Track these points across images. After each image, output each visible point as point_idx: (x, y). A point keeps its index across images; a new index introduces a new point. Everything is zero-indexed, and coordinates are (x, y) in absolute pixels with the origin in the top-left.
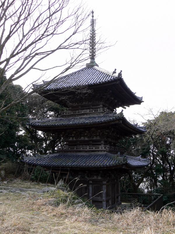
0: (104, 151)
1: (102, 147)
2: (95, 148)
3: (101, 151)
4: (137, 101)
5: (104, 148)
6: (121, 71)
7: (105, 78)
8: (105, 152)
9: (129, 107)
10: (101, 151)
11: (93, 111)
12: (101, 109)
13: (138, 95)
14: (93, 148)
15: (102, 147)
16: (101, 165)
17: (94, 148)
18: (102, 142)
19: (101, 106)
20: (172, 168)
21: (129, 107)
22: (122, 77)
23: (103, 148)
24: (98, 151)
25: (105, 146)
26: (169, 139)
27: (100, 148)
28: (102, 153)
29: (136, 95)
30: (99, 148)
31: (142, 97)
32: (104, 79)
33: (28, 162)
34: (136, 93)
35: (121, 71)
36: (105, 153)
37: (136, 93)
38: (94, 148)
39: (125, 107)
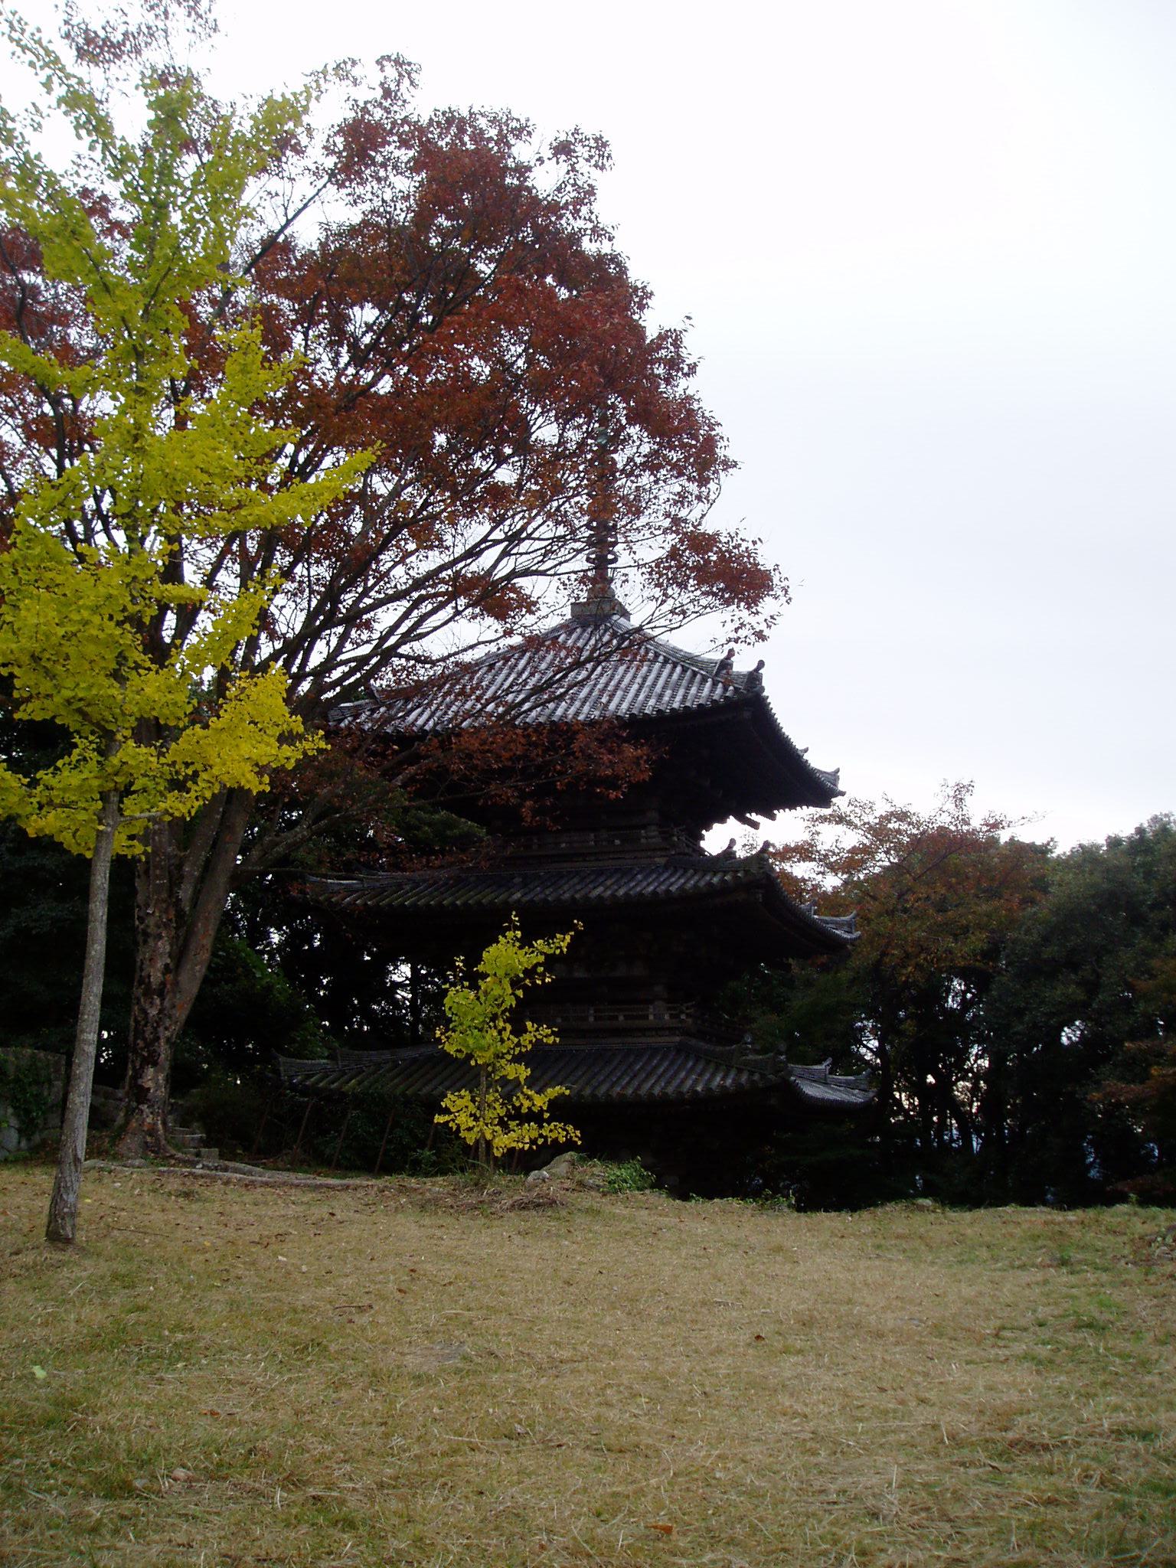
0: (672, 1031)
1: (658, 1013)
2: (626, 1017)
3: (658, 1030)
4: (813, 789)
5: (671, 1016)
6: (761, 664)
7: (681, 692)
8: (674, 1035)
9: (773, 817)
10: (658, 1030)
11: (617, 842)
12: (653, 831)
13: (818, 760)
14: (616, 1018)
15: (658, 1013)
16: (670, 1090)
17: (621, 1018)
18: (658, 989)
19: (653, 815)
20: (975, 1144)
21: (773, 817)
22: (763, 689)
23: (667, 1017)
24: (643, 1031)
25: (674, 1009)
26: (958, 985)
27: (651, 1017)
28: (659, 1039)
29: (806, 757)
30: (646, 1017)
31: (838, 771)
32: (679, 698)
33: (300, 1082)
34: (806, 750)
35: (761, 664)
36: (678, 1039)
37: (806, 750)
38: (621, 1018)
39: (754, 817)
